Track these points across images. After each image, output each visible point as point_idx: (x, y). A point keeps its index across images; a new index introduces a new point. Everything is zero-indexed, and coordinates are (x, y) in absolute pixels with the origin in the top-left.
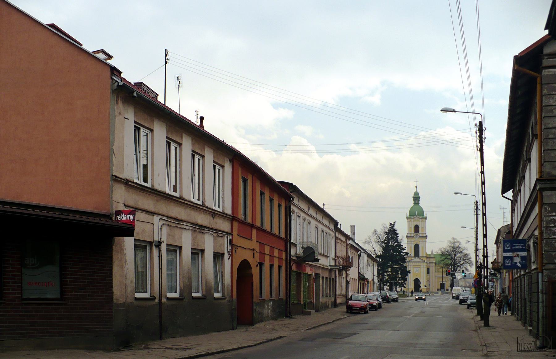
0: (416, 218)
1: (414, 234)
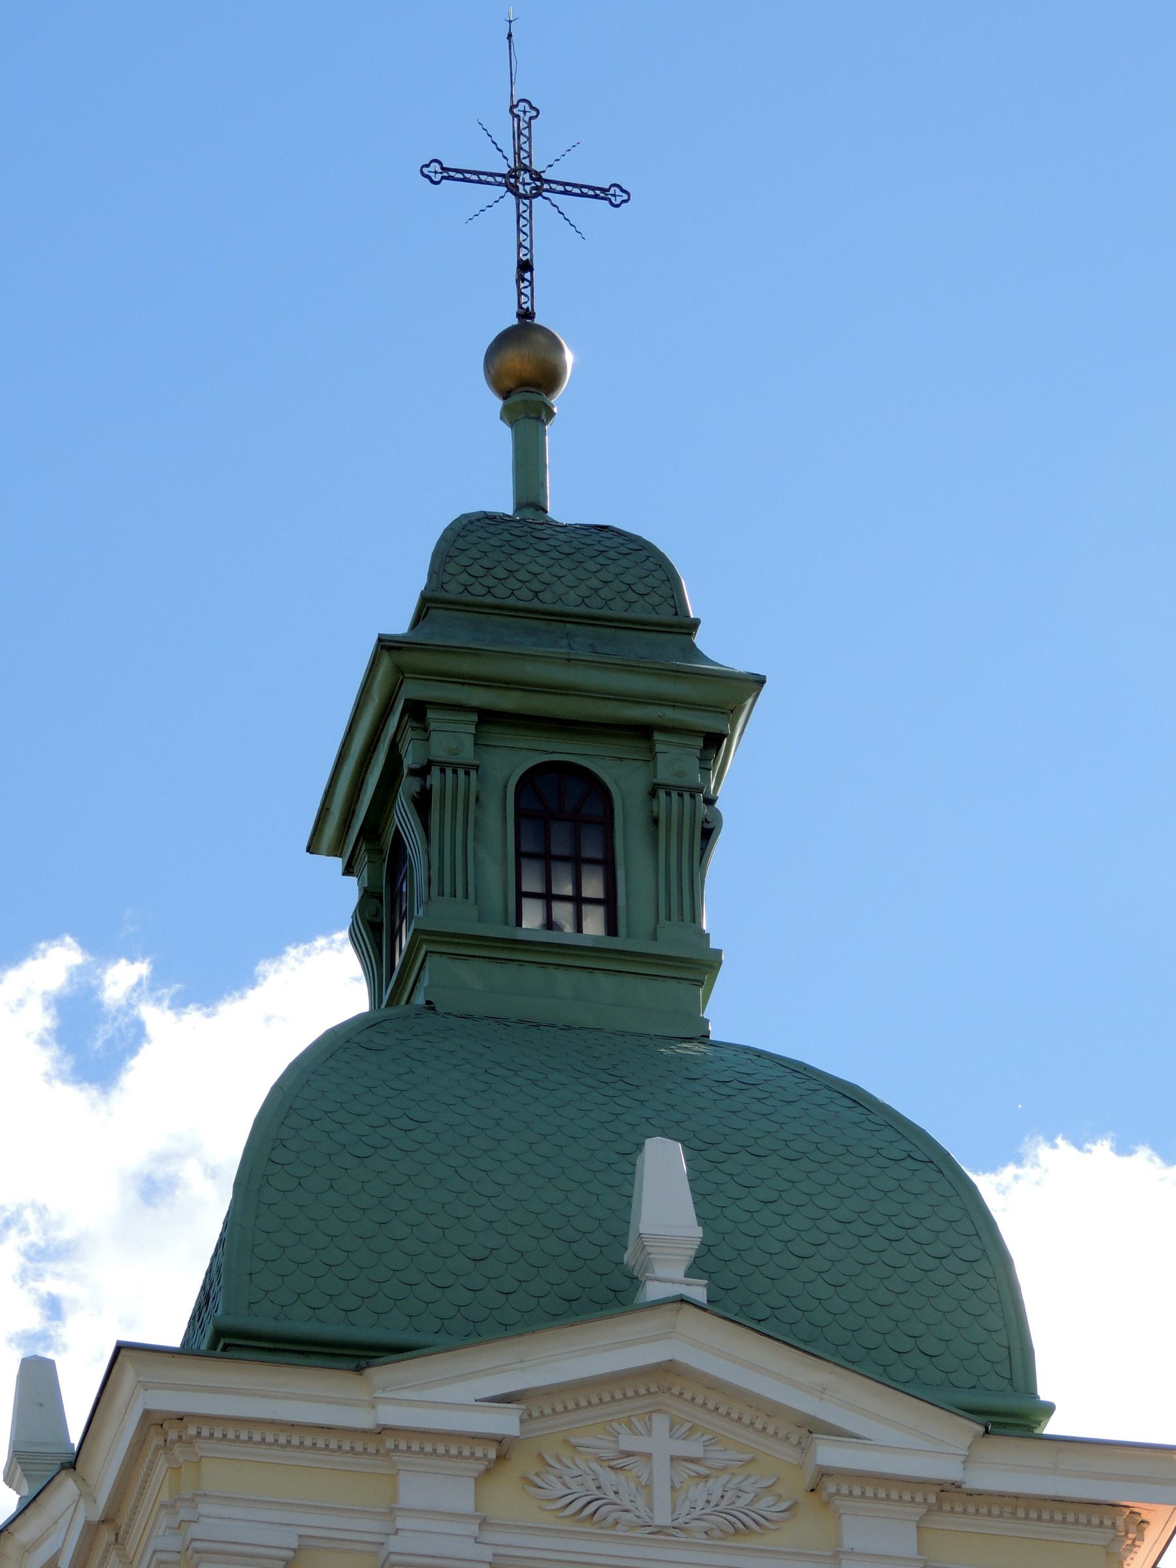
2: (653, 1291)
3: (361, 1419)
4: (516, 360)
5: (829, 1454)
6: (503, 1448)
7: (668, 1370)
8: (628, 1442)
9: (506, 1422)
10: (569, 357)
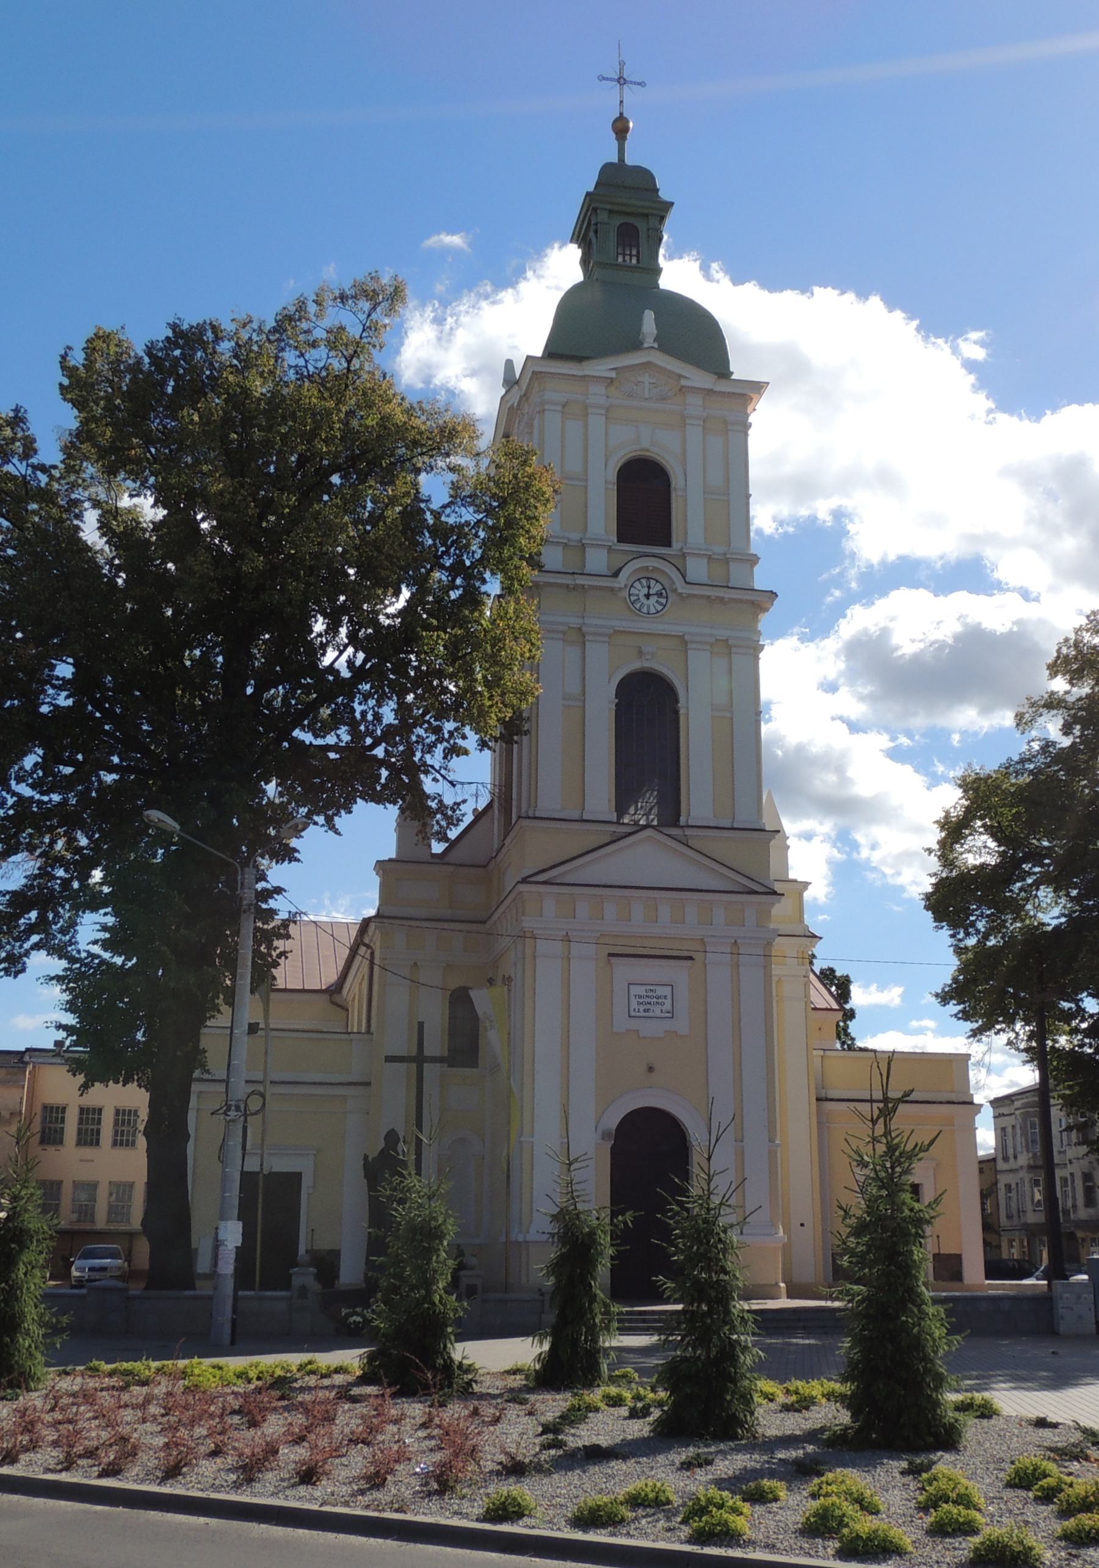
0: (646, 379)
1: (610, 548)
2: (646, 345)
3: (581, 373)
4: (619, 124)
5: (684, 382)
6: (612, 380)
7: (649, 363)
8: (640, 379)
9: (613, 375)
10: (631, 125)
